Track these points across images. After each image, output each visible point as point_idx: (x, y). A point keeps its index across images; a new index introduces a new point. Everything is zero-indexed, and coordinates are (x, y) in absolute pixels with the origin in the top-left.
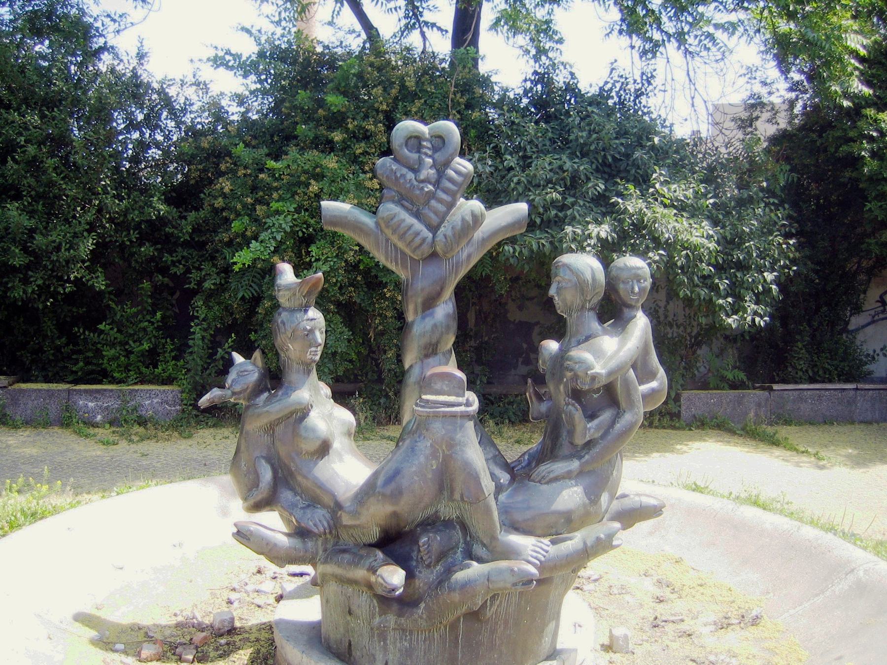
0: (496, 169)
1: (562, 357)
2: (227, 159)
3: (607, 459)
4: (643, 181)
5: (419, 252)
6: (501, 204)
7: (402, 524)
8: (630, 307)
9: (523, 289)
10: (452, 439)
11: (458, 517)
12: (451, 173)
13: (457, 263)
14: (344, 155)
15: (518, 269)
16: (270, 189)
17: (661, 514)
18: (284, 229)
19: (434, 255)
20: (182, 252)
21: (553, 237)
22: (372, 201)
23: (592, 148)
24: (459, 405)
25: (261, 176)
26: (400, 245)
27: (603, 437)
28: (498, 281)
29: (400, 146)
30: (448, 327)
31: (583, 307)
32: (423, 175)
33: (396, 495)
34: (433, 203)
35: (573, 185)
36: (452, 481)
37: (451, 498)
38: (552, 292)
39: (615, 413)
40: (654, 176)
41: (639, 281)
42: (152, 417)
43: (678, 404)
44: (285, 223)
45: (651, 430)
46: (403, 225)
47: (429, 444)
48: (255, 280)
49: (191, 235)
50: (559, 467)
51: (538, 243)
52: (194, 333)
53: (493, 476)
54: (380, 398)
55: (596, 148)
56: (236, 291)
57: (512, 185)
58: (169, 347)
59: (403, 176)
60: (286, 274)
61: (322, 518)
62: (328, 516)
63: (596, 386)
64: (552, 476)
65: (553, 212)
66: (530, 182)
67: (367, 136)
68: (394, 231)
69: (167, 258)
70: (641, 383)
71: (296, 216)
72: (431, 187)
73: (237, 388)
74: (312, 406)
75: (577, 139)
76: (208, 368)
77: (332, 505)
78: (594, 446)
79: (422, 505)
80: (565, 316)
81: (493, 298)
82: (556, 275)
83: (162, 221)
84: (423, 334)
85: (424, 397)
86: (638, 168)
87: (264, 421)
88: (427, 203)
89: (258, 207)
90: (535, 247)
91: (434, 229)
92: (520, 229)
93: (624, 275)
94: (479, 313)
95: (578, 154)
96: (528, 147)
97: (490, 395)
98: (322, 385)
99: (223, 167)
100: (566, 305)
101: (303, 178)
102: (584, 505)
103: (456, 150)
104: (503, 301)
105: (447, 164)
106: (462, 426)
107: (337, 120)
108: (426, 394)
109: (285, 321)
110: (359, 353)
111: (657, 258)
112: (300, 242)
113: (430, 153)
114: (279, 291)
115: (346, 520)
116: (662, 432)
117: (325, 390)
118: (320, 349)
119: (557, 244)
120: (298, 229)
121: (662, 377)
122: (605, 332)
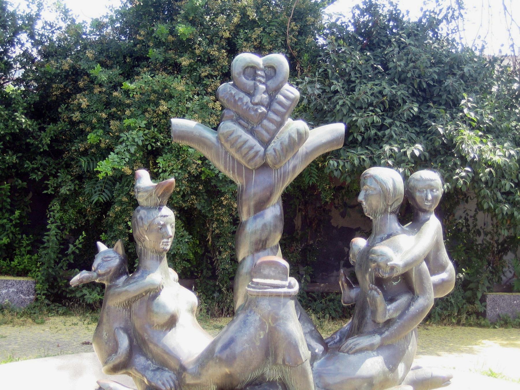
0: (324, 91)
1: (368, 252)
2: (86, 77)
3: (404, 335)
4: (454, 105)
5: (252, 163)
6: (327, 122)
7: (235, 383)
8: (425, 211)
9: (345, 198)
10: (277, 314)
11: (280, 379)
12: (280, 97)
13: (285, 173)
14: (190, 77)
15: (341, 181)
16: (120, 105)
17: (448, 384)
18: (137, 142)
19: (265, 166)
20: (41, 160)
21: (372, 153)
22: (213, 119)
23: (409, 75)
24: (283, 287)
25: (115, 94)
26: (237, 156)
27: (400, 317)
28: (324, 189)
29: (239, 74)
30: (275, 226)
31: (386, 211)
32: (257, 99)
33: (230, 360)
34: (265, 122)
35: (391, 107)
36: (276, 348)
37: (275, 363)
38: (361, 198)
39: (410, 297)
40: (463, 102)
41: (432, 190)
42: (8, 304)
43: (483, 304)
44: (137, 136)
45: (459, 327)
46: (239, 140)
47: (258, 318)
48: (107, 186)
49: (49, 146)
50: (364, 341)
51: (359, 158)
52: (49, 230)
53: (309, 347)
54: (214, 292)
55: (412, 76)
56: (90, 195)
57: (338, 107)
58: (25, 243)
59: (241, 99)
60: (144, 179)
61: (169, 379)
62: (174, 377)
63: (395, 275)
64: (358, 347)
65: (373, 132)
66: (353, 105)
67: (210, 61)
68: (232, 145)
69: (28, 164)
70: (433, 273)
71: (147, 131)
72: (264, 109)
73: (101, 271)
74: (163, 287)
75: (395, 67)
76: (60, 262)
77: (177, 367)
78: (393, 324)
79: (251, 368)
80: (371, 218)
81: (318, 205)
82: (364, 184)
83: (25, 133)
84: (255, 232)
85: (255, 280)
86: (450, 94)
87: (123, 298)
88: (260, 122)
89: (112, 122)
90: (356, 162)
91: (265, 144)
92: (338, 145)
93: (420, 185)
94: (305, 219)
95: (396, 80)
96: (352, 74)
97: (313, 292)
98: (171, 271)
99: (81, 84)
100: (371, 208)
101: (153, 97)
102: (384, 373)
103: (285, 78)
104: (327, 208)
105: (277, 90)
106: (285, 304)
107: (184, 46)
108: (256, 277)
109: (143, 216)
110: (195, 254)
111: (463, 174)
112: (148, 154)
113: (263, 80)
114: (138, 192)
115: (189, 380)
116: (468, 329)
117: (174, 275)
118: (170, 240)
119: (376, 160)
120: (147, 143)
121: (451, 269)
122: (404, 232)
